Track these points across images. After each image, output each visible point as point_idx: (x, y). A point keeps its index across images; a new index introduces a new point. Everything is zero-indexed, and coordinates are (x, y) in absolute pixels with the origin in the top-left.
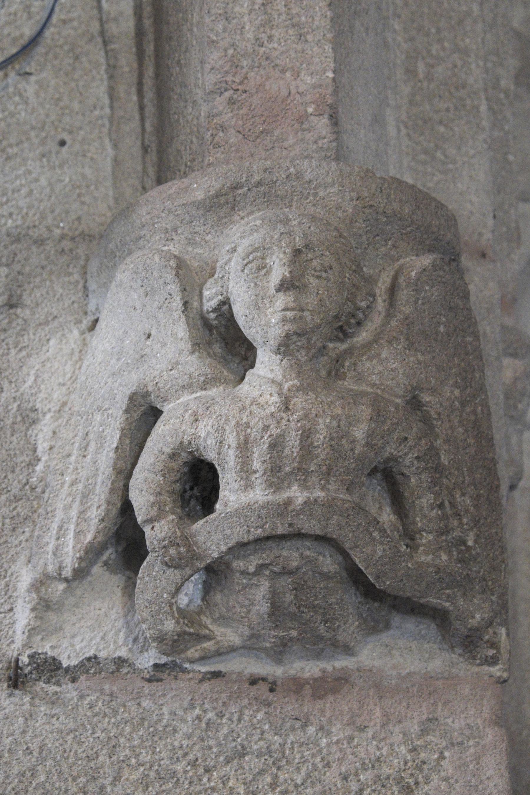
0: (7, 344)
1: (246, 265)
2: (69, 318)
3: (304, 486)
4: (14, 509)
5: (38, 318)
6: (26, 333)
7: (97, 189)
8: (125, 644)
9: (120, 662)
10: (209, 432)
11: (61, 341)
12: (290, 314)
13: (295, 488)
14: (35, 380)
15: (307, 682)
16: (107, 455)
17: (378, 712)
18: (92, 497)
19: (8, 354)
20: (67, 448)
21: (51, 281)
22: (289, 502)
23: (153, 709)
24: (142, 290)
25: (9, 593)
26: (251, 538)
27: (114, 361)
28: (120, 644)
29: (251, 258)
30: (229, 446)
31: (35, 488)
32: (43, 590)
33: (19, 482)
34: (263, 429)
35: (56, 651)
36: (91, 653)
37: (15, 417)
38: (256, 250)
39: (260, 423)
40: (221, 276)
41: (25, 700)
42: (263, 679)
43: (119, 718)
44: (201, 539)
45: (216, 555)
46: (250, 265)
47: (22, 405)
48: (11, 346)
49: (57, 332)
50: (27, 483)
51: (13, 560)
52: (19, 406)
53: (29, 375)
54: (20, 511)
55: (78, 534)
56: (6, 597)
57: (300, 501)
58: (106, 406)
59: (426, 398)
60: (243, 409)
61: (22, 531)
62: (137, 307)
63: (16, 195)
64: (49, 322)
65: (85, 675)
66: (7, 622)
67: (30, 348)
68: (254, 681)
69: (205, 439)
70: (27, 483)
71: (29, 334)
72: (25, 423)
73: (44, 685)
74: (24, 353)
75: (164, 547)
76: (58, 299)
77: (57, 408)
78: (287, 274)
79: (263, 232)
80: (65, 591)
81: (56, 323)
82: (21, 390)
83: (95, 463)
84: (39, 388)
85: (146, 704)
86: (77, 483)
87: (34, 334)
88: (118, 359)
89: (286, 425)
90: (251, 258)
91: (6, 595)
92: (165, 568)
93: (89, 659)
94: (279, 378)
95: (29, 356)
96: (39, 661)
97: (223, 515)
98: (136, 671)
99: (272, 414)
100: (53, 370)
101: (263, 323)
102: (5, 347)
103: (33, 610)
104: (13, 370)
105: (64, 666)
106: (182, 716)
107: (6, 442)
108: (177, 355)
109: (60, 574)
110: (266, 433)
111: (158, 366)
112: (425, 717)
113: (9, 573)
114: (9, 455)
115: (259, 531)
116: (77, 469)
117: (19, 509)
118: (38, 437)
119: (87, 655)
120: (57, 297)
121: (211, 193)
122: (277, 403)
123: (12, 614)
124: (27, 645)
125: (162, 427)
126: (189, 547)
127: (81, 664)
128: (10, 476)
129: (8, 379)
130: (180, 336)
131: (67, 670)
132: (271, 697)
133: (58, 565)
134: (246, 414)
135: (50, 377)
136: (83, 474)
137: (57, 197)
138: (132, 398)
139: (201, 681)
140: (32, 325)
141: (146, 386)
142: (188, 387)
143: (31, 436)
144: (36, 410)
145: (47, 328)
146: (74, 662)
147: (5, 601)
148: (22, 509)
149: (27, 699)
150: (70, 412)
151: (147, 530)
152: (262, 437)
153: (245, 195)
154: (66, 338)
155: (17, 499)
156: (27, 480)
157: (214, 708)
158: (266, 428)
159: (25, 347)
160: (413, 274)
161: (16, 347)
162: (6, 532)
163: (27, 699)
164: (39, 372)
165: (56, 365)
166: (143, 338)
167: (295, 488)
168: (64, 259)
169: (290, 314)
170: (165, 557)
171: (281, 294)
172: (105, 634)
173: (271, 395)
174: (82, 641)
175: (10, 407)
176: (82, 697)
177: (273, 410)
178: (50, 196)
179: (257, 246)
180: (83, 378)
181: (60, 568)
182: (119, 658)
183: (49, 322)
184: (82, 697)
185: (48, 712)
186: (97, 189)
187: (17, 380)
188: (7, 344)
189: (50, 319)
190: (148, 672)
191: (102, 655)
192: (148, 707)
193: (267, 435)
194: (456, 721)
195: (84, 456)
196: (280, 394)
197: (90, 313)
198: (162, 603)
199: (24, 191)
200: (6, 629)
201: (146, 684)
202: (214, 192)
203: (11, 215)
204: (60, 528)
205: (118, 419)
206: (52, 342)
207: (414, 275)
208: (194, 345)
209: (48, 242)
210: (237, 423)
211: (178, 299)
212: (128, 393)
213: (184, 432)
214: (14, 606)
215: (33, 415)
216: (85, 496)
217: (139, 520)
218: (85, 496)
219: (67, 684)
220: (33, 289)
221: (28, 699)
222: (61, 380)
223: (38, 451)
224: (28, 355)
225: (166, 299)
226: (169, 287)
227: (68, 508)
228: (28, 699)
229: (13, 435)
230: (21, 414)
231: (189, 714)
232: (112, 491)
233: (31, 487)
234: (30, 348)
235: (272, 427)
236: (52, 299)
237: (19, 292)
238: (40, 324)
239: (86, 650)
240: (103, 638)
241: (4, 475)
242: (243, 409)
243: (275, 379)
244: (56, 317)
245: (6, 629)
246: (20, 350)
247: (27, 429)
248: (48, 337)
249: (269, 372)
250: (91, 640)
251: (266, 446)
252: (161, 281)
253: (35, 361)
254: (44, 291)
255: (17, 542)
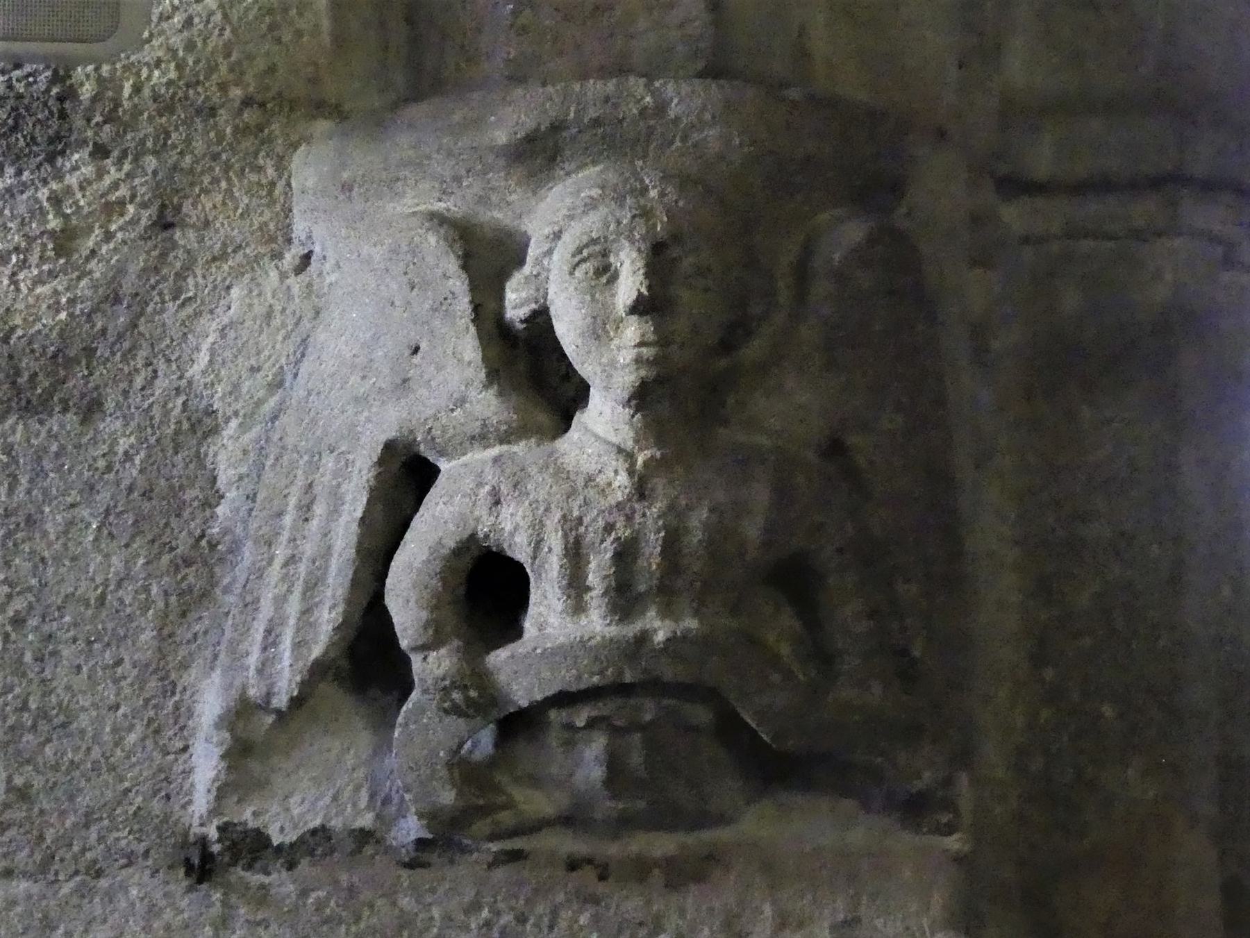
0: (160, 294)
1: (578, 264)
2: (262, 250)
3: (667, 611)
4: (184, 578)
5: (211, 247)
6: (190, 272)
7: (300, 14)
8: (370, 807)
9: (363, 837)
10: (518, 525)
11: (251, 291)
12: (647, 352)
13: (652, 613)
14: (211, 361)
15: (656, 863)
16: (346, 528)
17: (768, 910)
18: (322, 588)
19: (163, 311)
20: (276, 502)
21: (229, 180)
22: (643, 638)
23: (416, 910)
24: (405, 279)
25: (182, 722)
26: (582, 686)
27: (354, 379)
28: (363, 807)
29: (585, 253)
30: (550, 550)
31: (216, 546)
32: (241, 725)
33: (190, 533)
34: (605, 529)
35: (261, 819)
36: (317, 822)
37: (179, 422)
38: (594, 242)
39: (600, 519)
40: (534, 273)
41: (214, 899)
42: (589, 861)
43: (362, 925)
44: (502, 678)
45: (524, 703)
46: (584, 266)
47: (190, 403)
48: (167, 298)
49: (243, 274)
50: (202, 536)
51: (184, 666)
52: (185, 404)
53: (198, 349)
54: (193, 580)
55: (298, 645)
56: (177, 727)
57: (660, 637)
58: (343, 449)
59: (853, 440)
60: (572, 493)
61: (197, 616)
62: (397, 303)
63: (165, 25)
64: (229, 254)
65: (308, 858)
66: (181, 768)
67: (199, 301)
68: (573, 865)
69: (512, 534)
70: (202, 536)
71: (195, 277)
72: (196, 433)
73: (242, 873)
74: (189, 310)
75: (444, 689)
76: (242, 214)
77: (249, 409)
78: (644, 291)
79: (603, 211)
80: (273, 726)
81: (239, 257)
82: (188, 375)
83: (326, 535)
84: (217, 375)
85: (404, 902)
86: (295, 563)
87: (204, 277)
88: (364, 378)
89: (639, 524)
90: (585, 253)
91: (176, 724)
92: (441, 713)
93: (314, 832)
94: (629, 444)
95: (198, 314)
96: (235, 836)
97: (539, 651)
98: (388, 850)
99: (618, 505)
100: (240, 343)
101: (604, 360)
102: (157, 299)
103: (223, 757)
104: (172, 340)
105: (275, 843)
106: (463, 922)
107: (166, 465)
108: (463, 388)
109: (268, 703)
110: (610, 534)
111: (432, 401)
112: (841, 917)
113: (179, 688)
114: (171, 487)
115: (596, 679)
116: (295, 540)
117: (191, 579)
118: (219, 458)
119: (312, 825)
120: (240, 211)
121: (519, 136)
122: (626, 487)
123: (187, 755)
124: (214, 812)
125: (441, 506)
126: (482, 688)
127: (301, 840)
128: (174, 523)
129: (164, 355)
130: (467, 358)
131: (280, 849)
132: (601, 888)
133: (264, 690)
134: (578, 502)
135: (236, 357)
136: (308, 549)
137: (234, 31)
138: (389, 446)
139: (491, 866)
140: (200, 262)
141: (411, 432)
142: (482, 438)
143: (206, 455)
144: (213, 412)
145: (226, 267)
146: (291, 837)
147: (175, 735)
148: (192, 577)
149: (217, 896)
150: (280, 444)
151: (416, 661)
152: (602, 541)
153: (573, 138)
154: (259, 285)
155: (188, 562)
156: (203, 531)
157: (512, 909)
158: (609, 528)
159: (190, 298)
160: (837, 256)
161: (175, 298)
162: (171, 618)
163: (217, 896)
164: (216, 346)
165: (245, 334)
166: (407, 352)
167: (652, 613)
168: (248, 144)
169: (647, 352)
170: (445, 702)
171: (634, 318)
172: (338, 792)
173: (616, 472)
174: (303, 802)
175: (171, 405)
176: (304, 893)
177: (620, 499)
178: (222, 29)
179: (594, 235)
180: (302, 393)
181: (269, 695)
182: (362, 830)
183: (229, 254)
184: (304, 893)
185: (251, 918)
186: (300, 14)
187: (180, 357)
188: (160, 294)
189: (229, 250)
190: (408, 852)
191: (336, 823)
192: (409, 908)
193: (612, 538)
194: (890, 923)
195: (307, 520)
196: (631, 472)
197: (296, 241)
198: (436, 764)
199: (177, 19)
200: (179, 781)
201: (405, 873)
202: (523, 133)
203: (158, 63)
204: (268, 632)
205: (364, 472)
206: (235, 292)
207: (837, 259)
208: (488, 375)
209: (222, 111)
210: (564, 516)
211: (467, 300)
212: (383, 438)
213: (478, 520)
214: (191, 743)
215: (208, 421)
216: (312, 586)
217: (404, 644)
218: (312, 586)
219: (279, 872)
220: (199, 196)
221: (218, 895)
222: (253, 362)
223: (219, 483)
224: (196, 314)
225: (445, 299)
226: (451, 282)
227: (280, 601)
228: (218, 895)
229: (177, 453)
230: (189, 419)
231: (473, 919)
232: (355, 583)
233: (209, 542)
234: (199, 301)
235: (618, 525)
236: (231, 214)
237: (175, 200)
238: (214, 259)
239: (308, 817)
240: (335, 798)
241: (164, 521)
242: (572, 493)
243: (622, 446)
244: (240, 247)
245: (179, 781)
246: (183, 305)
247: (199, 444)
248: (227, 283)
249: (613, 433)
250: (317, 799)
251: (609, 555)
252: (439, 272)
253: (210, 327)
254: (219, 198)
255: (190, 636)
